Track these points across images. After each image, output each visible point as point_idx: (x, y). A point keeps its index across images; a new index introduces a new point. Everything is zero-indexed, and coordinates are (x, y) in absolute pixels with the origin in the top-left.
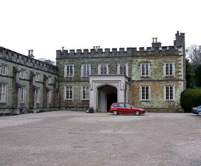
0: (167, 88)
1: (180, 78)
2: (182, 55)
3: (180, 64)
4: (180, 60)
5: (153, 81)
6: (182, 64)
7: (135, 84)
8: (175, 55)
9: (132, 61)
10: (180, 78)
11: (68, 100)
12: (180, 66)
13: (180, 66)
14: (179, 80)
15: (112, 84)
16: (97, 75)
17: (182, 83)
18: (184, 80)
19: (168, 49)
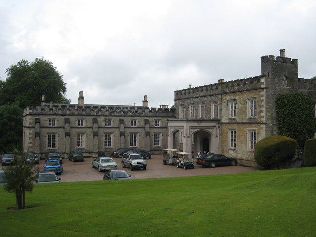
0: (54, 144)
1: (262, 120)
2: (264, 88)
3: (263, 101)
4: (262, 96)
5: (238, 124)
6: (264, 100)
7: (224, 127)
8: (257, 89)
9: (221, 100)
10: (262, 120)
11: (155, 147)
12: (262, 104)
13: (262, 104)
14: (260, 124)
15: (208, 130)
16: (178, 120)
17: (263, 127)
18: (268, 122)
19: (107, 108)
